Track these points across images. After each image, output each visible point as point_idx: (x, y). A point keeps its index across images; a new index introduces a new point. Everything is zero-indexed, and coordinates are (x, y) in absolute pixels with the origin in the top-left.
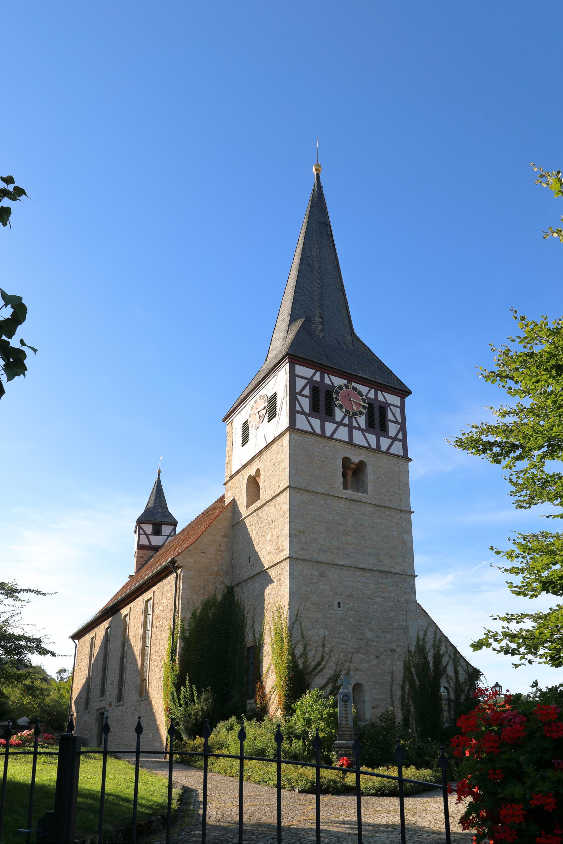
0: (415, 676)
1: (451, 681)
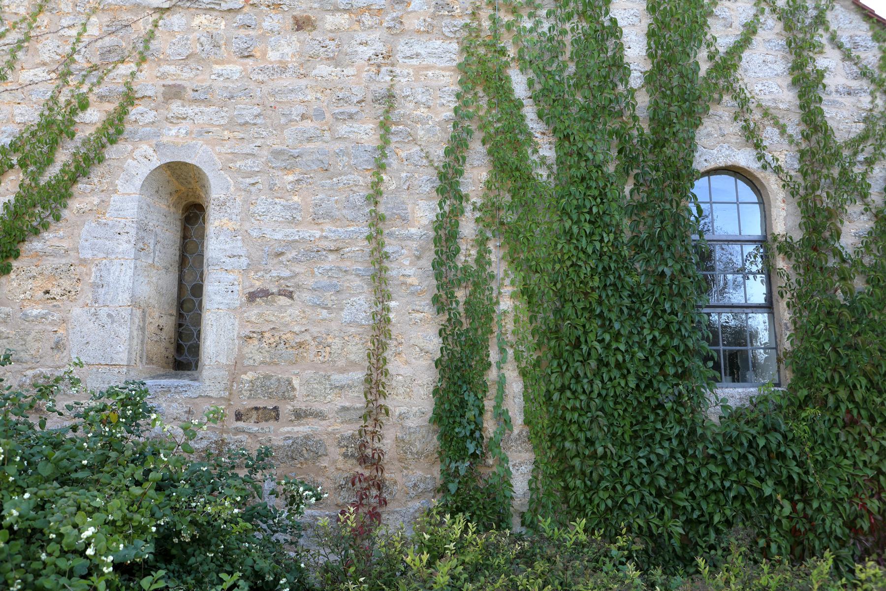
0: (529, 112)
1: (770, 135)
